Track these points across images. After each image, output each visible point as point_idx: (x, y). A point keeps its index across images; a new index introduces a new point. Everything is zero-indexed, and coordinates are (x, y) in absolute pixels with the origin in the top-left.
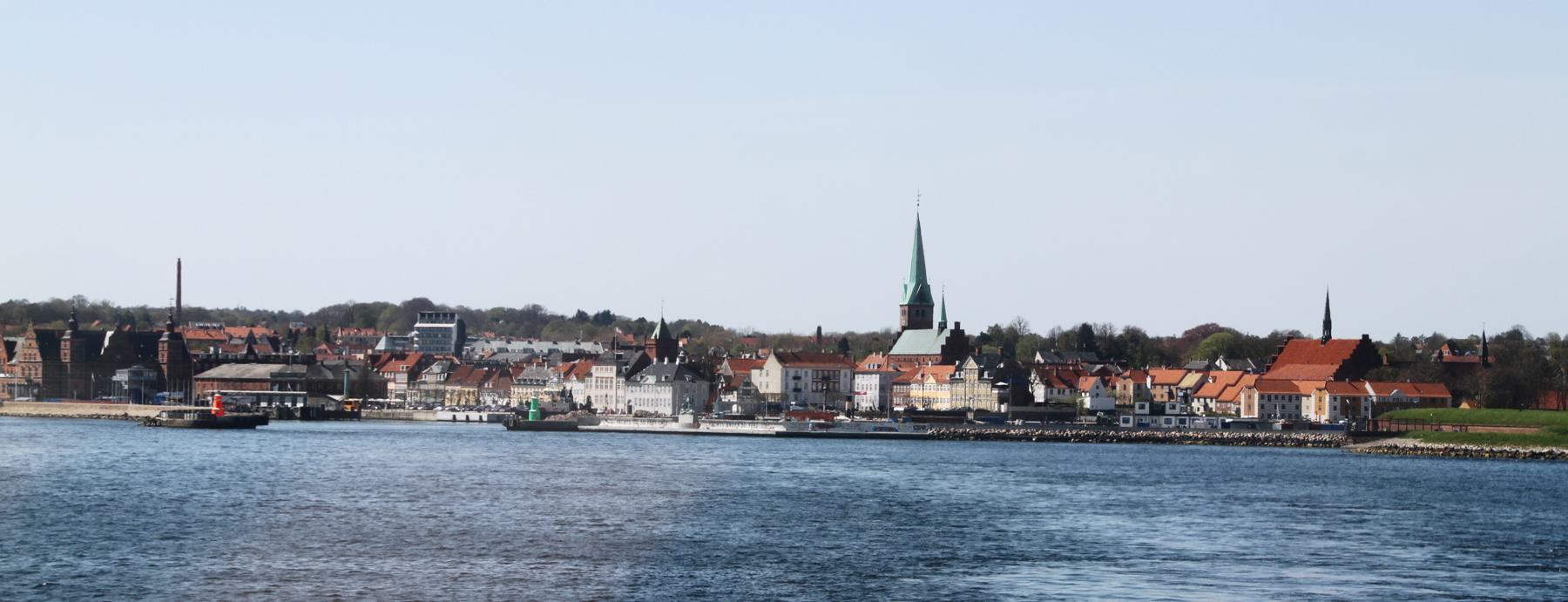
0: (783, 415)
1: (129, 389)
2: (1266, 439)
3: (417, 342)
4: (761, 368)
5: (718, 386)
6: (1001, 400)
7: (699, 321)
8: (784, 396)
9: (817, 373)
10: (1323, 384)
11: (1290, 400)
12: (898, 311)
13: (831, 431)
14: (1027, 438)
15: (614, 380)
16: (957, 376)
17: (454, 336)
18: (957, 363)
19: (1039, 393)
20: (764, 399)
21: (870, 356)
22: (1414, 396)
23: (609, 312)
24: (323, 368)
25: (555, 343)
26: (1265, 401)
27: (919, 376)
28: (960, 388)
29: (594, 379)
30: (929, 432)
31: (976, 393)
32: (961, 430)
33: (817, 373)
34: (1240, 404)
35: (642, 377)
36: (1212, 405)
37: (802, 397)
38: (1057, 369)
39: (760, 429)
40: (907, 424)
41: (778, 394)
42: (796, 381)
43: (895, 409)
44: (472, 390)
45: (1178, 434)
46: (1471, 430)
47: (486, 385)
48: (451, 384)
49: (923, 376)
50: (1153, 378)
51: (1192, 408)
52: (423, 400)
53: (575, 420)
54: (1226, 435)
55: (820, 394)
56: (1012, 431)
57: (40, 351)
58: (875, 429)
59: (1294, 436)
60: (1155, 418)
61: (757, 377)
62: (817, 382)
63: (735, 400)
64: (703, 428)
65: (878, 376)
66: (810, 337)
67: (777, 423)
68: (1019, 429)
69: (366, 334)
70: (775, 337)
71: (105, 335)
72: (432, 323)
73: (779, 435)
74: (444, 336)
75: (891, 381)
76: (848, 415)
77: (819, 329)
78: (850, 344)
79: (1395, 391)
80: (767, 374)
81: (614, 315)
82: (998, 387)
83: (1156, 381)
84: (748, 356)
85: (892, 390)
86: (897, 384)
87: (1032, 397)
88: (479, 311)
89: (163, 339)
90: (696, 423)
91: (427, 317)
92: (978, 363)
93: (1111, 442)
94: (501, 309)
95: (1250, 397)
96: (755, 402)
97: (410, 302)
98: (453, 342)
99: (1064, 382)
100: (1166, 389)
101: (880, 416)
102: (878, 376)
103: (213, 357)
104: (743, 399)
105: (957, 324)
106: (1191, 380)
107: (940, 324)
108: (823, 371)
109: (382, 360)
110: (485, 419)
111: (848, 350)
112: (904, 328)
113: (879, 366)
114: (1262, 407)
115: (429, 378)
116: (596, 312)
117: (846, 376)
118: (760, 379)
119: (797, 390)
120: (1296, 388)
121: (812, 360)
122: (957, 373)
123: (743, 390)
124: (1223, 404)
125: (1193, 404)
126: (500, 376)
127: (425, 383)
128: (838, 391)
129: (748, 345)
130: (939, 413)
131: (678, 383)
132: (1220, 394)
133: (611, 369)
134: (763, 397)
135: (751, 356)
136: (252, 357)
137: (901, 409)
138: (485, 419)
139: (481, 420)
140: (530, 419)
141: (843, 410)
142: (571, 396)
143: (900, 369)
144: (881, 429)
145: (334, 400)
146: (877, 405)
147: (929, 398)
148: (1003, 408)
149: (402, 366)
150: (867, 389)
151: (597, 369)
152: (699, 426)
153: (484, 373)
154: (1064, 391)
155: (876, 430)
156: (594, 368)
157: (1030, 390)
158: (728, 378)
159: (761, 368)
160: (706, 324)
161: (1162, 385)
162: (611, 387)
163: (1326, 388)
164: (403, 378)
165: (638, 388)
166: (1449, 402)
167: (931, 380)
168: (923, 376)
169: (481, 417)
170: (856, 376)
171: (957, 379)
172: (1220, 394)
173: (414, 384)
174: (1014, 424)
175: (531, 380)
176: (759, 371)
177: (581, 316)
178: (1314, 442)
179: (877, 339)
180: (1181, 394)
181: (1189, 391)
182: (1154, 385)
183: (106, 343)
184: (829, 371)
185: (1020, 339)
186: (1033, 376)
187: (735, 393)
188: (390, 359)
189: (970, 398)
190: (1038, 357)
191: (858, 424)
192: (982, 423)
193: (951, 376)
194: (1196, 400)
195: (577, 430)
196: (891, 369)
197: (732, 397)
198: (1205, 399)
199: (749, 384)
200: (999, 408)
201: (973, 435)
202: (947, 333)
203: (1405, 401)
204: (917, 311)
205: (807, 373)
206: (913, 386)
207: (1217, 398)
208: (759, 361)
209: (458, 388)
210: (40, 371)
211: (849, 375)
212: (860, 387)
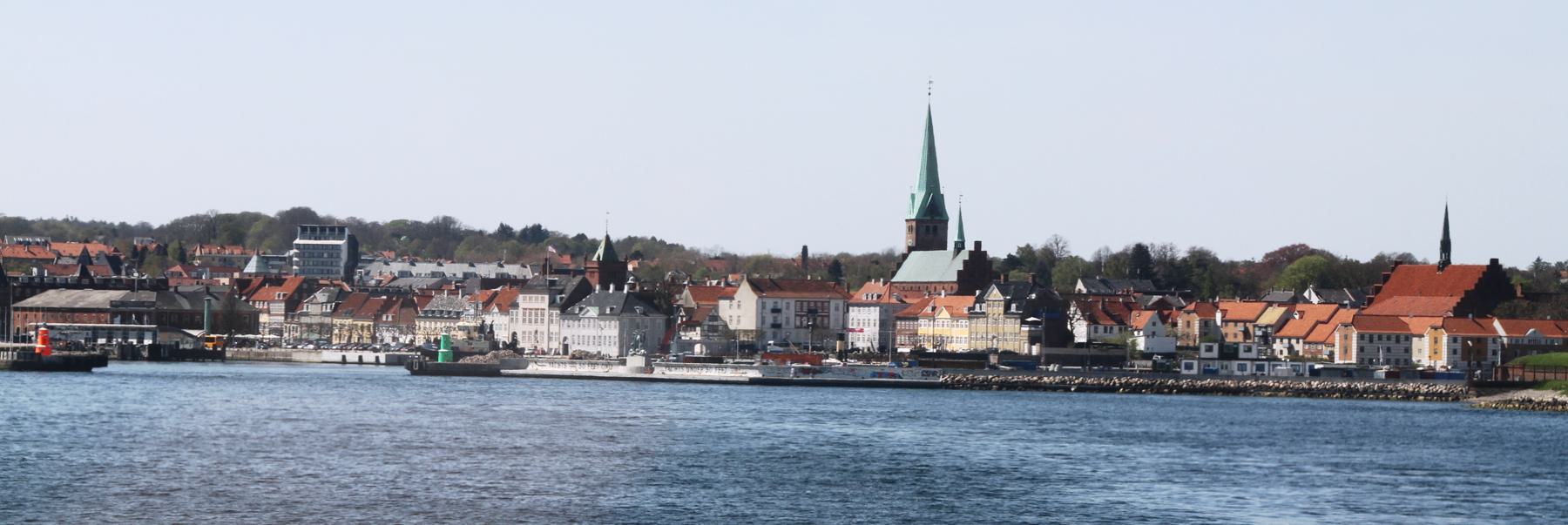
0: (758, 358)
2: (1365, 391)
4: (731, 298)
6: (1033, 340)
7: (654, 239)
8: (760, 333)
9: (802, 304)
10: (1439, 322)
12: (904, 227)
13: (818, 377)
14: (1063, 387)
15: (546, 312)
16: (977, 309)
17: (344, 255)
18: (978, 292)
19: (1081, 331)
20: (734, 338)
21: (868, 283)
23: (539, 226)
24: (176, 296)
25: (472, 265)
26: (1365, 343)
27: (928, 310)
28: (980, 325)
29: (520, 311)
30: (941, 379)
31: (1001, 331)
32: (981, 377)
33: (802, 304)
35: (581, 309)
37: (782, 334)
39: (728, 374)
40: (914, 369)
41: (752, 331)
42: (776, 315)
43: (899, 350)
44: (366, 324)
45: (1254, 384)
47: (384, 318)
49: (934, 309)
50: (1224, 312)
53: (496, 362)
54: (1315, 384)
55: (806, 330)
56: (1046, 379)
58: (874, 375)
59: (1401, 386)
60: (1225, 363)
61: (726, 310)
62: (802, 316)
63: (698, 338)
64: (658, 373)
65: (878, 308)
66: (793, 260)
67: (750, 366)
68: (1055, 377)
70: (749, 259)
72: (316, 239)
73: (753, 382)
74: (331, 256)
75: (895, 315)
77: (805, 249)
78: (843, 267)
79: (1531, 330)
80: (739, 306)
81: (546, 231)
82: (1028, 323)
83: (1227, 317)
84: (714, 282)
85: (894, 326)
86: (901, 319)
87: (1071, 336)
88: (375, 224)
90: (649, 367)
91: (327, 232)
92: (1004, 292)
93: (1170, 393)
94: (404, 222)
96: (724, 341)
98: (342, 264)
99: (1112, 318)
100: (1241, 327)
101: (879, 359)
102: (878, 308)
105: (978, 244)
106: (1272, 315)
107: (956, 243)
108: (809, 302)
110: (382, 360)
111: (841, 276)
112: (911, 249)
113: (879, 296)
114: (1361, 349)
115: (313, 309)
116: (523, 227)
117: (837, 309)
118: (730, 312)
119: (776, 326)
121: (794, 290)
122: (978, 305)
123: (709, 326)
125: (1275, 346)
126: (402, 306)
127: (306, 314)
128: (828, 327)
129: (715, 269)
130: (954, 355)
131: (626, 317)
133: (543, 299)
134: (732, 335)
135: (719, 283)
136: (86, 281)
137: (906, 350)
138: (382, 360)
139: (377, 362)
140: (440, 361)
142: (492, 331)
143: (904, 300)
144: (881, 375)
146: (876, 345)
147: (942, 337)
148: (1035, 350)
149: (278, 293)
150: (864, 326)
152: (652, 371)
154: (1111, 328)
155: (874, 376)
157: (1069, 327)
158: (689, 311)
159: (731, 298)
160: (662, 243)
161: (1236, 322)
163: (1443, 327)
164: (279, 308)
165: (576, 322)
167: (945, 314)
168: (934, 309)
169: (377, 358)
170: (851, 308)
171: (977, 313)
173: (293, 317)
174: (1048, 369)
175: (449, 312)
176: (728, 301)
177: (505, 231)
178: (1426, 394)
179: (877, 263)
180: (1259, 333)
181: (1269, 330)
184: (815, 302)
185: (1057, 263)
186: (1072, 309)
187: (698, 329)
188: (262, 285)
189: (994, 337)
190: (1080, 286)
191: (853, 369)
192: (1008, 368)
193: (970, 309)
194: (1278, 341)
196: (894, 300)
197: (695, 335)
198: (1290, 339)
199: (716, 318)
200: (1030, 350)
201: (996, 383)
202: (964, 255)
204: (927, 227)
205: (789, 305)
206: (922, 321)
207: (1304, 338)
208: (729, 289)
209: (349, 321)
212: (855, 321)
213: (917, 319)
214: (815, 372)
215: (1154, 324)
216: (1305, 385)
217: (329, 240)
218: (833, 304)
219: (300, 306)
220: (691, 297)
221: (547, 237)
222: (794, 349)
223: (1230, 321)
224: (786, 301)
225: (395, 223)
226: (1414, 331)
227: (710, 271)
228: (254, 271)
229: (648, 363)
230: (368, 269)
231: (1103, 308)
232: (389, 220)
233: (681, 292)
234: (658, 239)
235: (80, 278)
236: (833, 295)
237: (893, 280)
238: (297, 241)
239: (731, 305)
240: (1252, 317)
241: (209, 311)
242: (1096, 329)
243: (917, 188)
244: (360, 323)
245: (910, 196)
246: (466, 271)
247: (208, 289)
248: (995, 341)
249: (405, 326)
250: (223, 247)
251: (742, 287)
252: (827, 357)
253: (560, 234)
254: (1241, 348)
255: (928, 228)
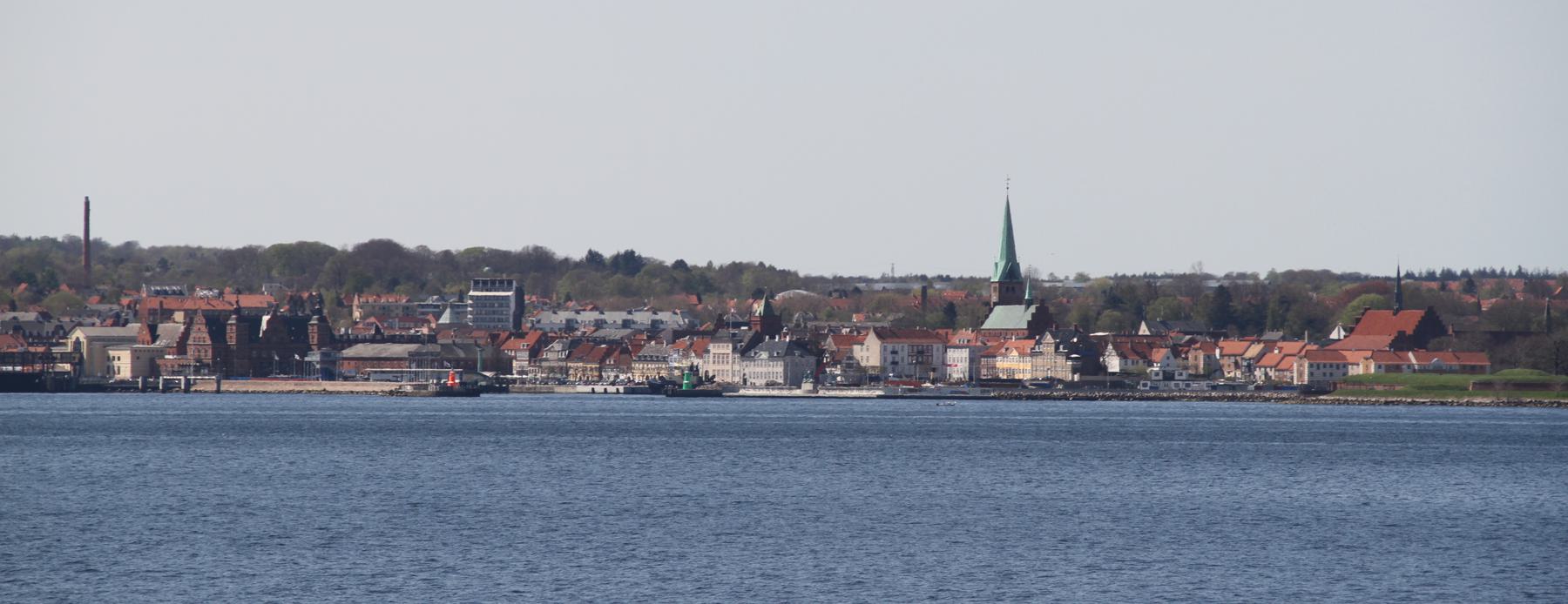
0: (882, 383)
1: (321, 368)
2: (1242, 397)
3: (471, 313)
4: (862, 344)
5: (823, 360)
6: (1074, 371)
7: (761, 264)
8: (883, 369)
10: (1369, 354)
11: (1318, 368)
15: (730, 355)
18: (1037, 338)
19: (1114, 364)
22: (1455, 363)
24: (455, 348)
27: (1003, 350)
28: (1039, 360)
29: (711, 355)
34: (1491, 373)
35: (756, 353)
36: (1272, 373)
37: (899, 369)
38: (1132, 342)
39: (864, 393)
41: (877, 367)
42: (894, 355)
44: (594, 366)
45: (1178, 394)
46: (1398, 388)
48: (572, 361)
49: (1007, 349)
50: (1222, 349)
51: (1255, 376)
52: (551, 375)
54: (1213, 394)
57: (210, 335)
59: (1262, 394)
60: (1166, 382)
62: (912, 356)
63: (839, 373)
64: (821, 393)
69: (388, 301)
71: (261, 320)
72: (487, 291)
73: (879, 397)
76: (933, 382)
78: (957, 309)
80: (868, 349)
81: (640, 257)
82: (1072, 359)
83: (1224, 352)
85: (980, 362)
86: (984, 357)
89: (312, 322)
90: (815, 390)
91: (481, 285)
93: (1129, 400)
94: (480, 250)
95: (1301, 365)
97: (365, 245)
99: (1138, 354)
103: (345, 337)
104: (845, 371)
106: (1255, 350)
109: (500, 339)
110: (621, 390)
113: (968, 341)
114: (1311, 374)
115: (550, 356)
117: (938, 350)
118: (862, 354)
119: (894, 363)
120: (1344, 358)
124: (1281, 373)
125: (1256, 373)
126: (621, 353)
127: (546, 360)
129: (838, 307)
131: (788, 358)
132: (1278, 364)
133: (728, 346)
134: (864, 370)
136: (378, 337)
140: (684, 388)
141: (929, 379)
142: (698, 370)
145: (485, 376)
146: (967, 375)
149: (523, 344)
150: (958, 362)
151: (714, 347)
152: (817, 392)
153: (604, 350)
154: (1137, 362)
156: (711, 345)
159: (862, 344)
160: (772, 269)
161: (1229, 356)
162: (728, 363)
163: (1371, 357)
164: (525, 355)
165: (753, 363)
166: (1488, 369)
167: (1015, 353)
168: (1007, 349)
169: (618, 389)
170: (948, 350)
172: (1278, 364)
173: (535, 362)
175: (657, 357)
176: (859, 346)
178: (1275, 399)
180: (1245, 364)
182: (1222, 355)
183: (264, 326)
188: (508, 338)
194: (1258, 369)
195: (723, 396)
196: (979, 344)
198: (1266, 368)
199: (851, 358)
200: (1073, 378)
203: (1444, 368)
205: (904, 348)
206: (999, 358)
209: (580, 364)
210: (210, 353)
211: (941, 349)
213: (995, 357)
214: (915, 391)
215: (1168, 358)
216: (1207, 395)
217: (498, 291)
218: (935, 346)
219: (540, 354)
220: (833, 344)
221: (644, 265)
222: (904, 379)
223: (1226, 355)
224: (901, 345)
225: (468, 251)
226: (1350, 361)
227: (834, 309)
228: (448, 322)
229: (815, 388)
230: (539, 317)
231: (1132, 347)
232: (462, 248)
233: (825, 340)
234: (767, 265)
235: (374, 336)
236: (936, 340)
237: (983, 327)
238: (471, 293)
239: (862, 350)
240: (1241, 352)
241: (481, 358)
242: (1126, 362)
243: (999, 258)
244: (589, 366)
245: (993, 264)
246: (624, 318)
247: (476, 342)
248: (1049, 372)
249: (625, 367)
250: (379, 296)
251: (869, 336)
252: (925, 383)
253: (657, 260)
254: (1176, 374)
255: (1007, 289)
